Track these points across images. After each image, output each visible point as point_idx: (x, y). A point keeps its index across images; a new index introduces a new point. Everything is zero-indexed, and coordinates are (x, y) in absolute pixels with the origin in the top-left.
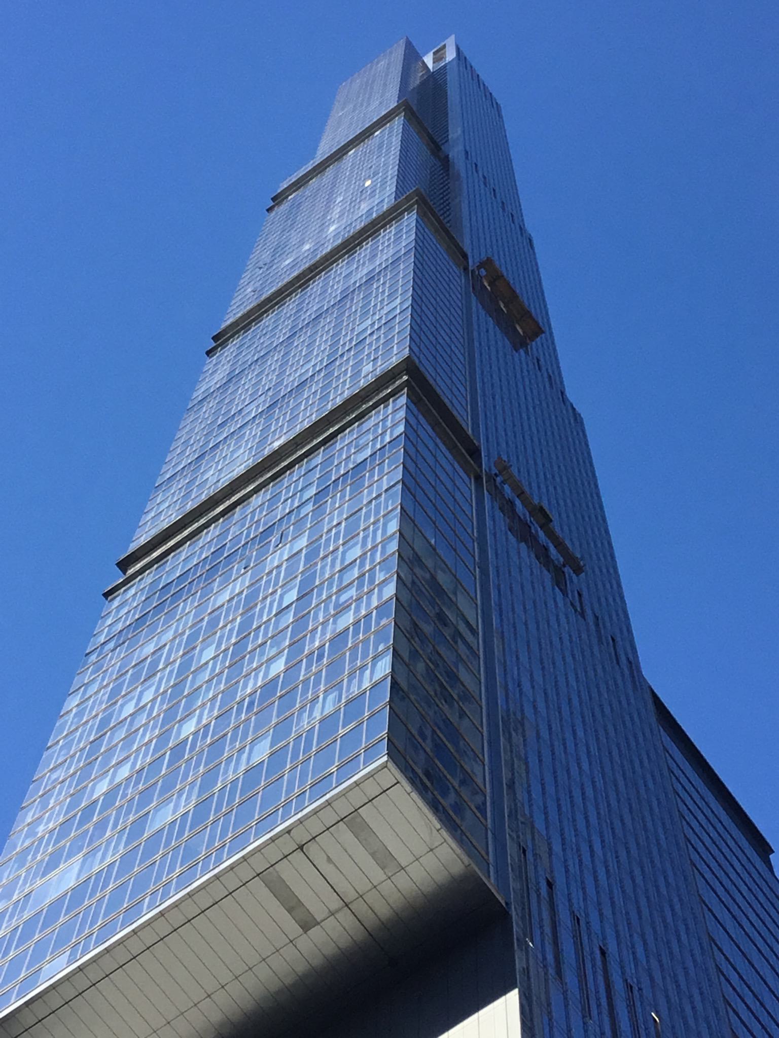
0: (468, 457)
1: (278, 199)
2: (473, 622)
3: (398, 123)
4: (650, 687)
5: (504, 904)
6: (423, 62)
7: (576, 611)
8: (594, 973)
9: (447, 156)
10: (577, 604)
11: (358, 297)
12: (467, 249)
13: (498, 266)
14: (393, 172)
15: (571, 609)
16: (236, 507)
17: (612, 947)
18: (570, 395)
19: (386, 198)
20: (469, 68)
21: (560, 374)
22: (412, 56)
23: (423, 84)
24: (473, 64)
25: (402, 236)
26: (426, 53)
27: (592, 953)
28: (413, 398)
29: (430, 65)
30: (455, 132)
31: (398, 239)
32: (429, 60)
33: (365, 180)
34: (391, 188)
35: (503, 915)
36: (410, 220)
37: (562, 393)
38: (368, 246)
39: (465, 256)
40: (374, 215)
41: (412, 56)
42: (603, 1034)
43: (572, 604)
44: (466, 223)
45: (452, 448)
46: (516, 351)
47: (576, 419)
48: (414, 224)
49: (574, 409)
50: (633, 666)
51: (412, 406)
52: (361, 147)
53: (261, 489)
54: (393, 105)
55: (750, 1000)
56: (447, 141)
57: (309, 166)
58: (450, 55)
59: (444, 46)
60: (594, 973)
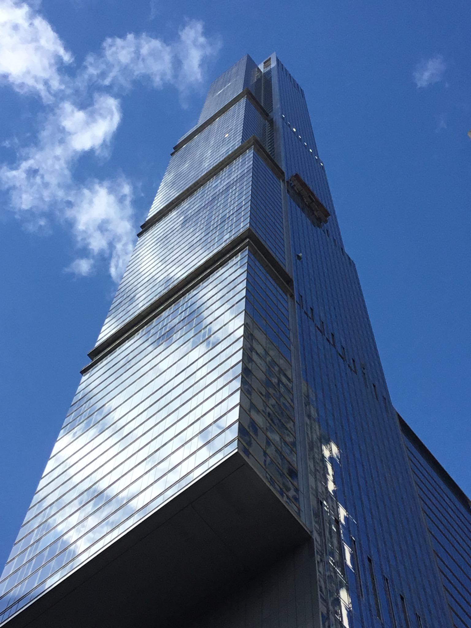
0: (285, 284)
1: (177, 148)
2: (290, 377)
3: (243, 102)
4: (399, 415)
5: (309, 533)
6: (258, 69)
7: (351, 370)
8: (364, 571)
9: (272, 119)
10: (352, 365)
11: (221, 199)
12: (284, 169)
13: (302, 178)
14: (240, 128)
15: (348, 370)
16: (153, 319)
17: (375, 558)
18: (346, 249)
19: (237, 142)
20: (284, 70)
21: (341, 239)
22: (251, 65)
23: (259, 80)
24: (288, 69)
25: (245, 164)
26: (260, 63)
27: (363, 561)
28: (252, 252)
29: (262, 70)
30: (277, 105)
31: (243, 164)
32: (261, 67)
33: (225, 134)
34: (239, 138)
35: (309, 539)
36: (250, 154)
37: (342, 249)
38: (226, 170)
39: (283, 173)
40: (230, 152)
41: (251, 65)
42: (402, 627)
43: (349, 366)
44: (283, 154)
45: (275, 279)
46: (319, 227)
47: (350, 263)
48: (252, 155)
49: (349, 258)
50: (386, 400)
51: (252, 257)
52: (223, 117)
53: (167, 308)
54: (240, 91)
55: (460, 588)
56: (272, 111)
57: (194, 129)
58: (273, 64)
59: (270, 58)
60: (364, 571)
